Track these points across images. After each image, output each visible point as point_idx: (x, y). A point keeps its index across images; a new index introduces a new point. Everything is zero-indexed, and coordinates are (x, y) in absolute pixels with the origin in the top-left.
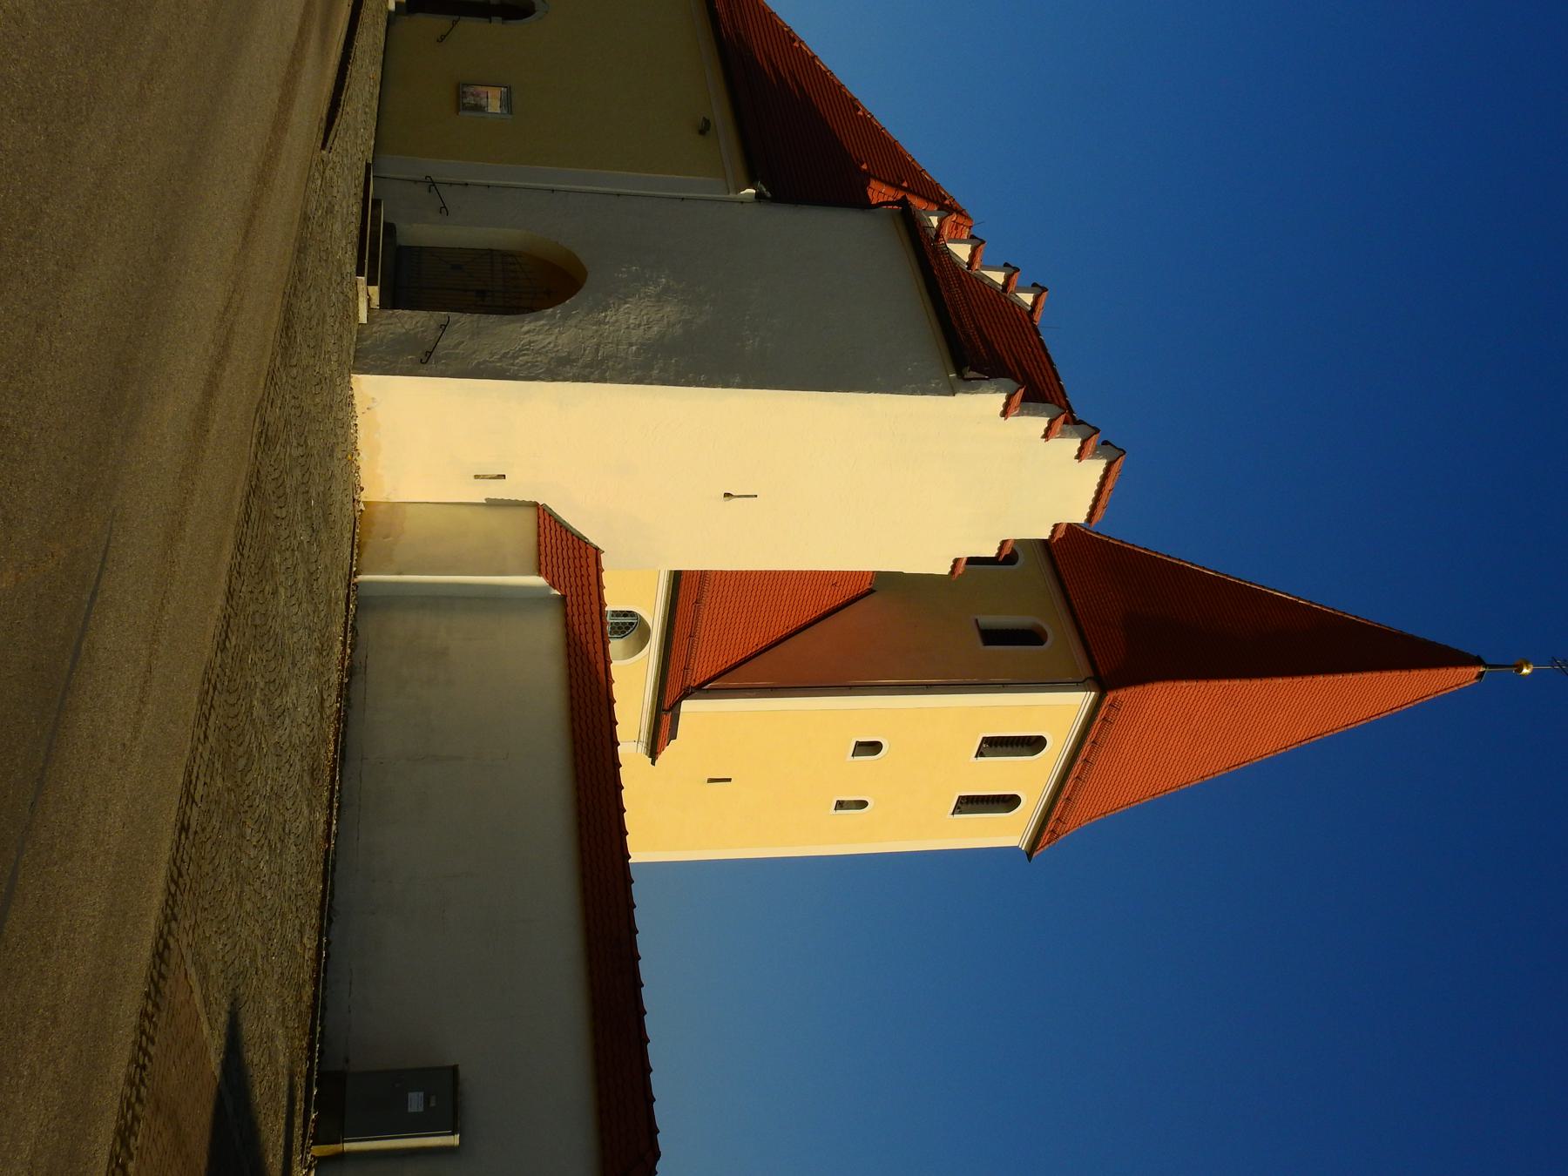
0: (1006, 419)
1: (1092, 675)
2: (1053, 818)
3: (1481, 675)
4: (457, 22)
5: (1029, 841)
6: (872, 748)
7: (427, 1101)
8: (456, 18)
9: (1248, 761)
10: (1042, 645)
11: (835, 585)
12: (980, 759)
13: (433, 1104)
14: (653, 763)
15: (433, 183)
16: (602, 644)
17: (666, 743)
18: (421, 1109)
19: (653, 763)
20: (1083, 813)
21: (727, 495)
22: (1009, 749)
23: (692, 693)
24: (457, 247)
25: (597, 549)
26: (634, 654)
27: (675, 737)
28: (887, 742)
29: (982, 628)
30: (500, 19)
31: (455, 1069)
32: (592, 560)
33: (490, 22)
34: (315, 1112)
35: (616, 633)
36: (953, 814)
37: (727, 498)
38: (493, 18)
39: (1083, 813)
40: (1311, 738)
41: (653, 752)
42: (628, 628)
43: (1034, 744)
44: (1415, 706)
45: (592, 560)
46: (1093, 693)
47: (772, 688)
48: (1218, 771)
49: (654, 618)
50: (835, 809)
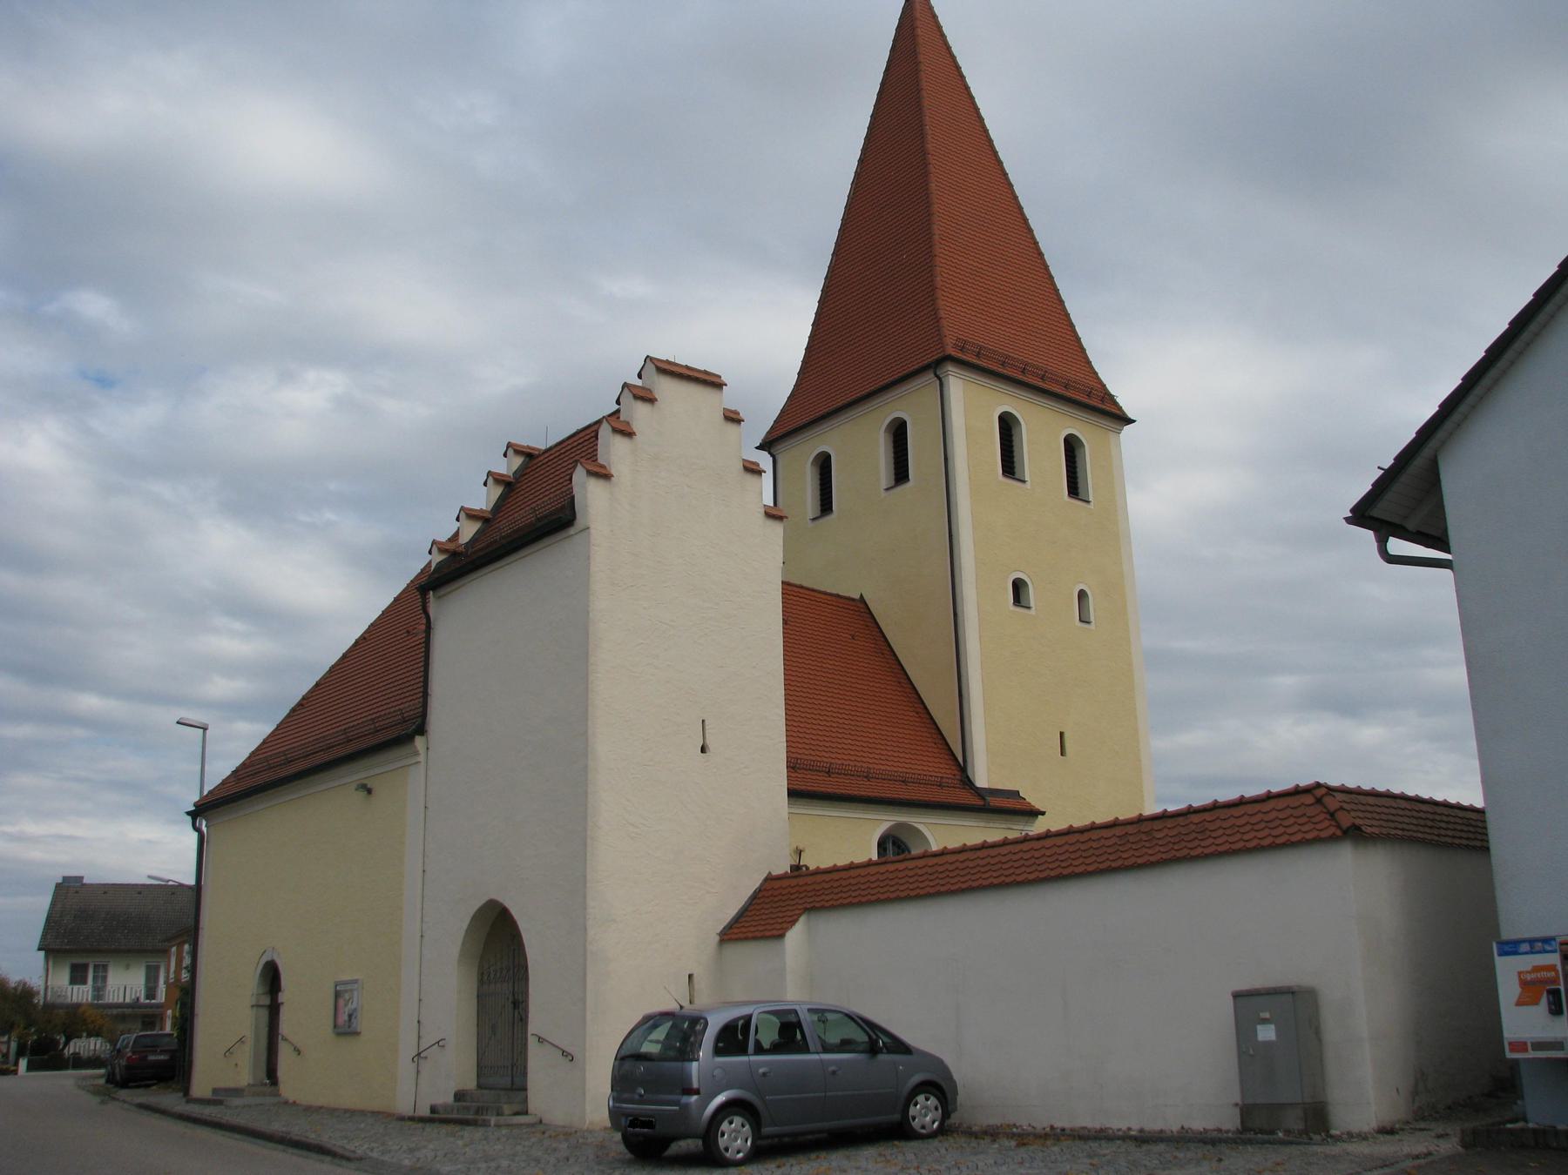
0: (612, 476)
2: (1087, 401)
4: (283, 1036)
6: (1018, 587)
7: (1265, 1021)
8: (280, 1037)
10: (905, 422)
13: (1267, 1015)
14: (1043, 813)
15: (419, 1054)
16: (852, 870)
18: (1273, 1027)
19: (1043, 813)
21: (703, 750)
24: (476, 1028)
25: (766, 880)
28: (1014, 574)
29: (893, 483)
30: (280, 994)
31: (1237, 996)
32: (777, 884)
33: (282, 1003)
34: (1277, 1134)
37: (707, 750)
38: (280, 1001)
41: (1034, 813)
43: (1007, 426)
45: (777, 884)
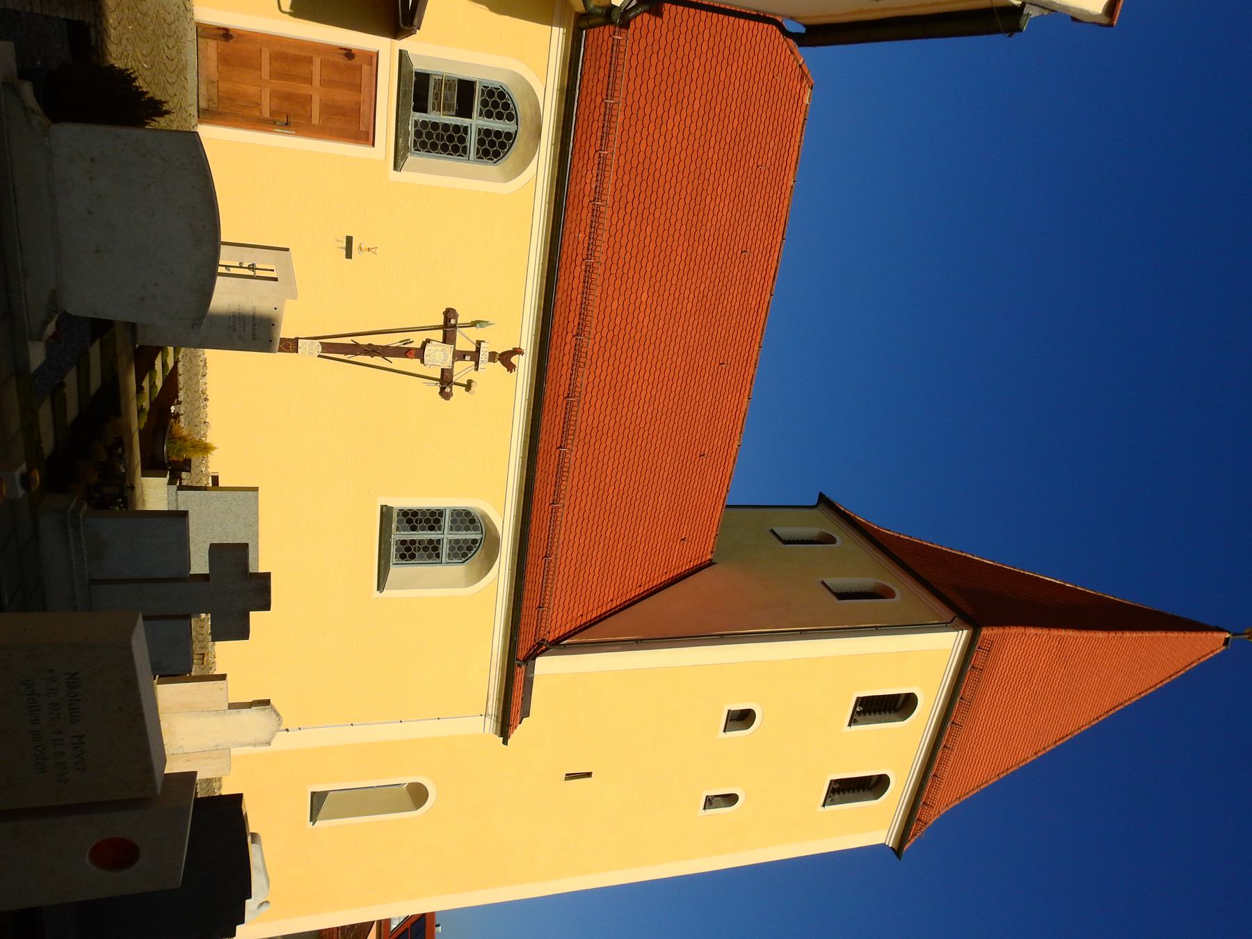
1: (955, 615)
3: (1227, 640)
5: (896, 834)
6: (741, 719)
9: (1070, 734)
10: (894, 598)
11: (684, 539)
12: (855, 728)
14: (505, 742)
17: (518, 722)
19: (505, 742)
20: (931, 816)
22: (878, 716)
23: (547, 649)
26: (481, 577)
27: (527, 714)
35: (456, 556)
36: (824, 805)
39: (944, 799)
40: (1115, 707)
42: (469, 549)
44: (1187, 672)
46: (965, 632)
47: (636, 640)
48: (1083, 726)
49: (504, 520)
50: (704, 809)
